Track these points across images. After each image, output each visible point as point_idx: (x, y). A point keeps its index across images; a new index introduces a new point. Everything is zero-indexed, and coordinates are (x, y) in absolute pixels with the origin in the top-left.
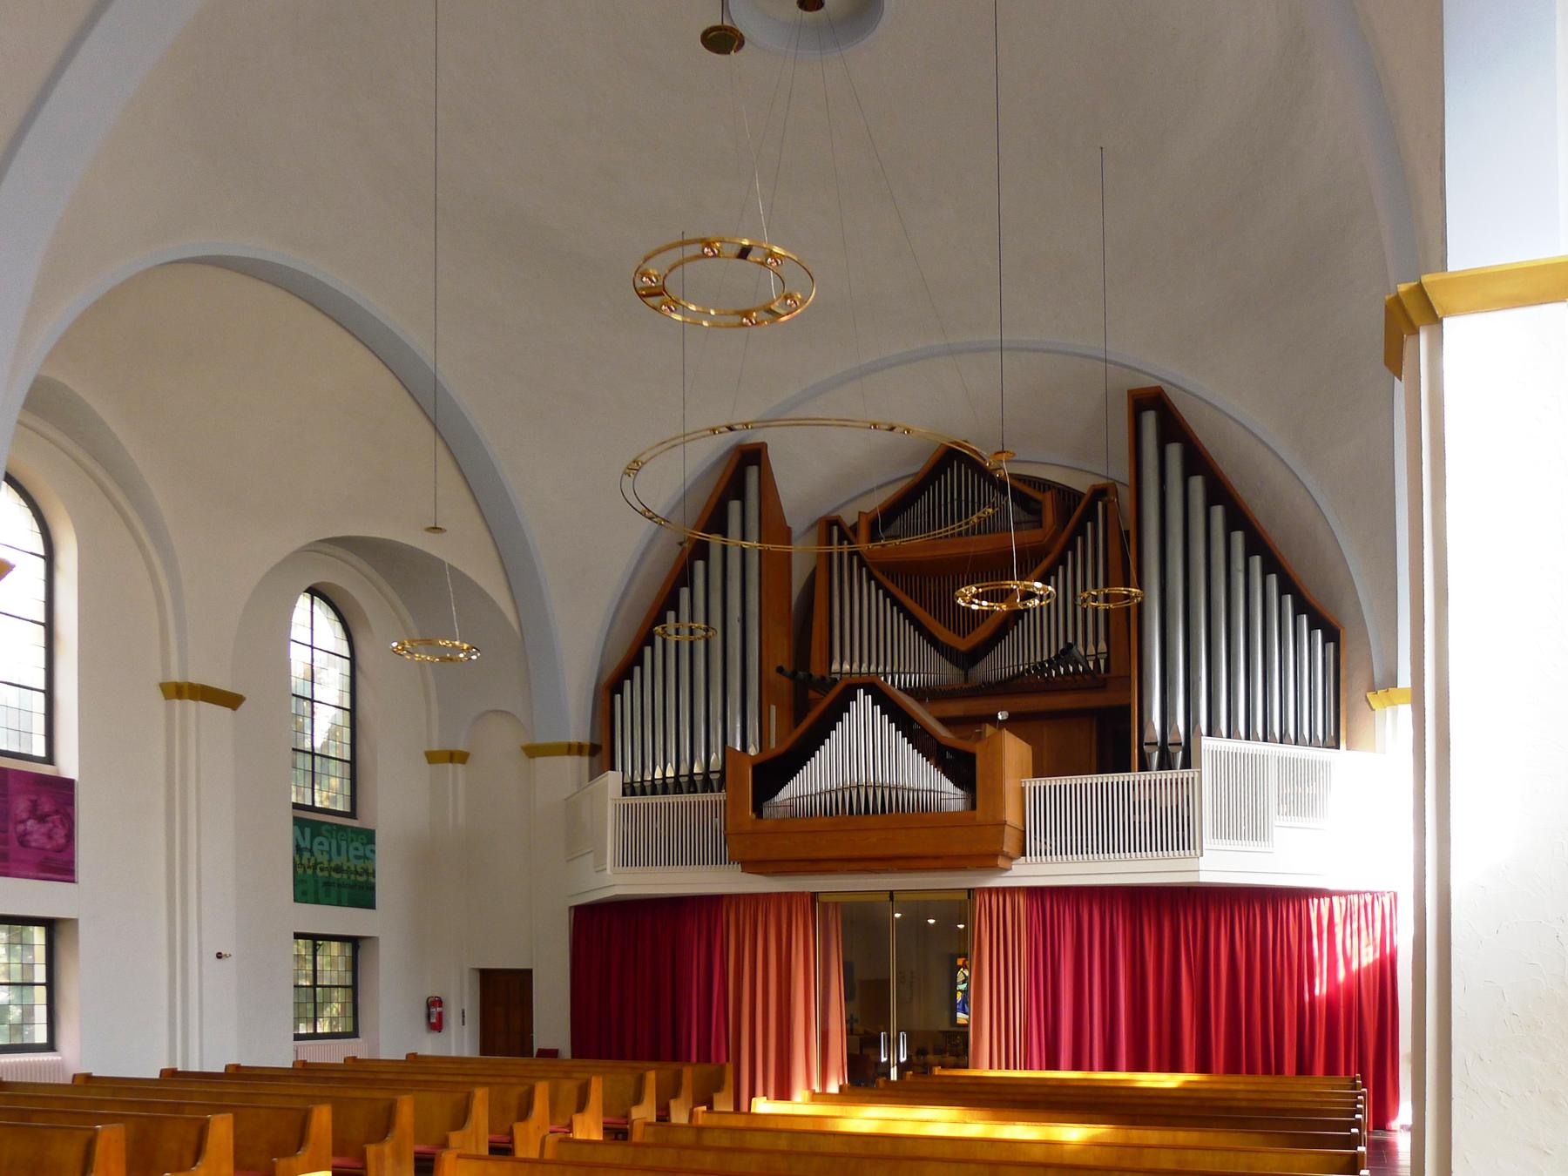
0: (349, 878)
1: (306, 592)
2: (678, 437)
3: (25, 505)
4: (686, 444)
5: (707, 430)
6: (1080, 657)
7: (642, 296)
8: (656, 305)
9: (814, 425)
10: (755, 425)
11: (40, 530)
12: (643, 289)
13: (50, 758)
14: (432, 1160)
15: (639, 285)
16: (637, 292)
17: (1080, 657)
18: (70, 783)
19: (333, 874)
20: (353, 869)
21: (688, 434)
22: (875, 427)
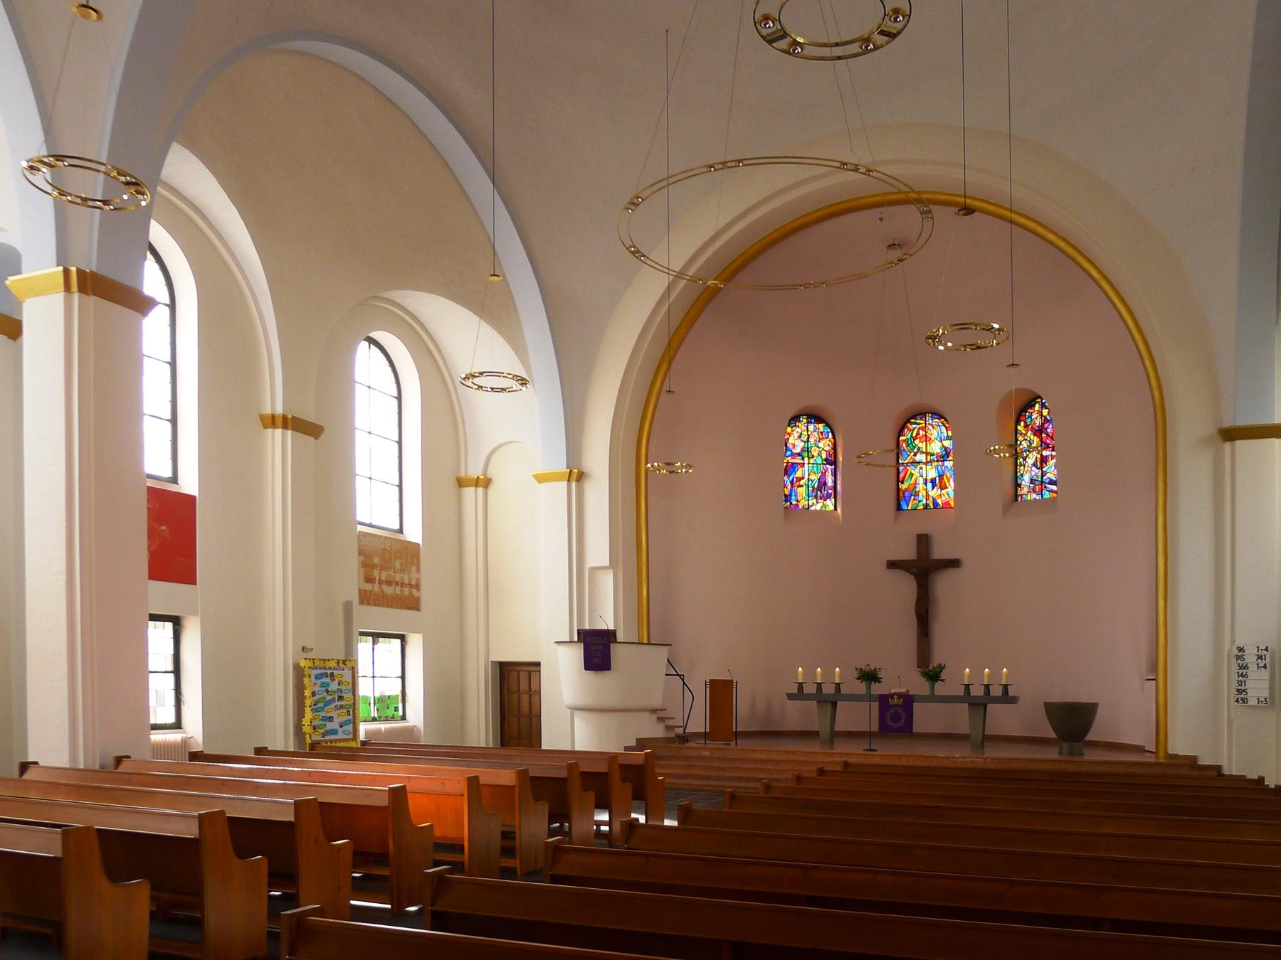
0: (402, 591)
1: (365, 340)
2: (663, 180)
3: (154, 260)
4: (670, 187)
5: (704, 166)
6: (1052, 754)
7: (770, 42)
8: (785, 48)
9: (827, 160)
10: (745, 162)
11: (166, 282)
12: (768, 35)
13: (174, 479)
14: (531, 745)
15: (765, 32)
16: (764, 39)
17: (1052, 754)
18: (191, 500)
19: (385, 587)
20: (406, 582)
21: (672, 176)
22: (633, 204)
